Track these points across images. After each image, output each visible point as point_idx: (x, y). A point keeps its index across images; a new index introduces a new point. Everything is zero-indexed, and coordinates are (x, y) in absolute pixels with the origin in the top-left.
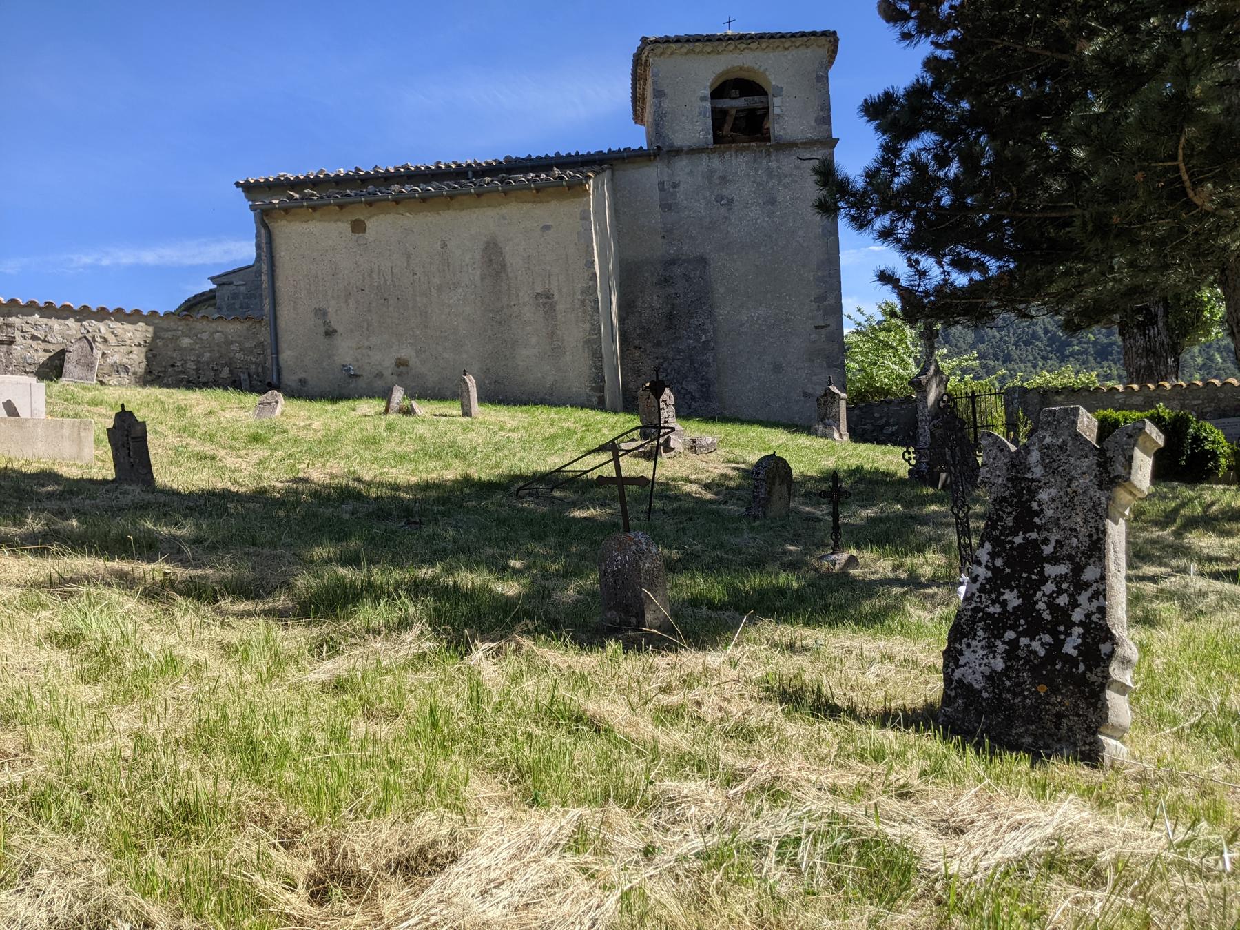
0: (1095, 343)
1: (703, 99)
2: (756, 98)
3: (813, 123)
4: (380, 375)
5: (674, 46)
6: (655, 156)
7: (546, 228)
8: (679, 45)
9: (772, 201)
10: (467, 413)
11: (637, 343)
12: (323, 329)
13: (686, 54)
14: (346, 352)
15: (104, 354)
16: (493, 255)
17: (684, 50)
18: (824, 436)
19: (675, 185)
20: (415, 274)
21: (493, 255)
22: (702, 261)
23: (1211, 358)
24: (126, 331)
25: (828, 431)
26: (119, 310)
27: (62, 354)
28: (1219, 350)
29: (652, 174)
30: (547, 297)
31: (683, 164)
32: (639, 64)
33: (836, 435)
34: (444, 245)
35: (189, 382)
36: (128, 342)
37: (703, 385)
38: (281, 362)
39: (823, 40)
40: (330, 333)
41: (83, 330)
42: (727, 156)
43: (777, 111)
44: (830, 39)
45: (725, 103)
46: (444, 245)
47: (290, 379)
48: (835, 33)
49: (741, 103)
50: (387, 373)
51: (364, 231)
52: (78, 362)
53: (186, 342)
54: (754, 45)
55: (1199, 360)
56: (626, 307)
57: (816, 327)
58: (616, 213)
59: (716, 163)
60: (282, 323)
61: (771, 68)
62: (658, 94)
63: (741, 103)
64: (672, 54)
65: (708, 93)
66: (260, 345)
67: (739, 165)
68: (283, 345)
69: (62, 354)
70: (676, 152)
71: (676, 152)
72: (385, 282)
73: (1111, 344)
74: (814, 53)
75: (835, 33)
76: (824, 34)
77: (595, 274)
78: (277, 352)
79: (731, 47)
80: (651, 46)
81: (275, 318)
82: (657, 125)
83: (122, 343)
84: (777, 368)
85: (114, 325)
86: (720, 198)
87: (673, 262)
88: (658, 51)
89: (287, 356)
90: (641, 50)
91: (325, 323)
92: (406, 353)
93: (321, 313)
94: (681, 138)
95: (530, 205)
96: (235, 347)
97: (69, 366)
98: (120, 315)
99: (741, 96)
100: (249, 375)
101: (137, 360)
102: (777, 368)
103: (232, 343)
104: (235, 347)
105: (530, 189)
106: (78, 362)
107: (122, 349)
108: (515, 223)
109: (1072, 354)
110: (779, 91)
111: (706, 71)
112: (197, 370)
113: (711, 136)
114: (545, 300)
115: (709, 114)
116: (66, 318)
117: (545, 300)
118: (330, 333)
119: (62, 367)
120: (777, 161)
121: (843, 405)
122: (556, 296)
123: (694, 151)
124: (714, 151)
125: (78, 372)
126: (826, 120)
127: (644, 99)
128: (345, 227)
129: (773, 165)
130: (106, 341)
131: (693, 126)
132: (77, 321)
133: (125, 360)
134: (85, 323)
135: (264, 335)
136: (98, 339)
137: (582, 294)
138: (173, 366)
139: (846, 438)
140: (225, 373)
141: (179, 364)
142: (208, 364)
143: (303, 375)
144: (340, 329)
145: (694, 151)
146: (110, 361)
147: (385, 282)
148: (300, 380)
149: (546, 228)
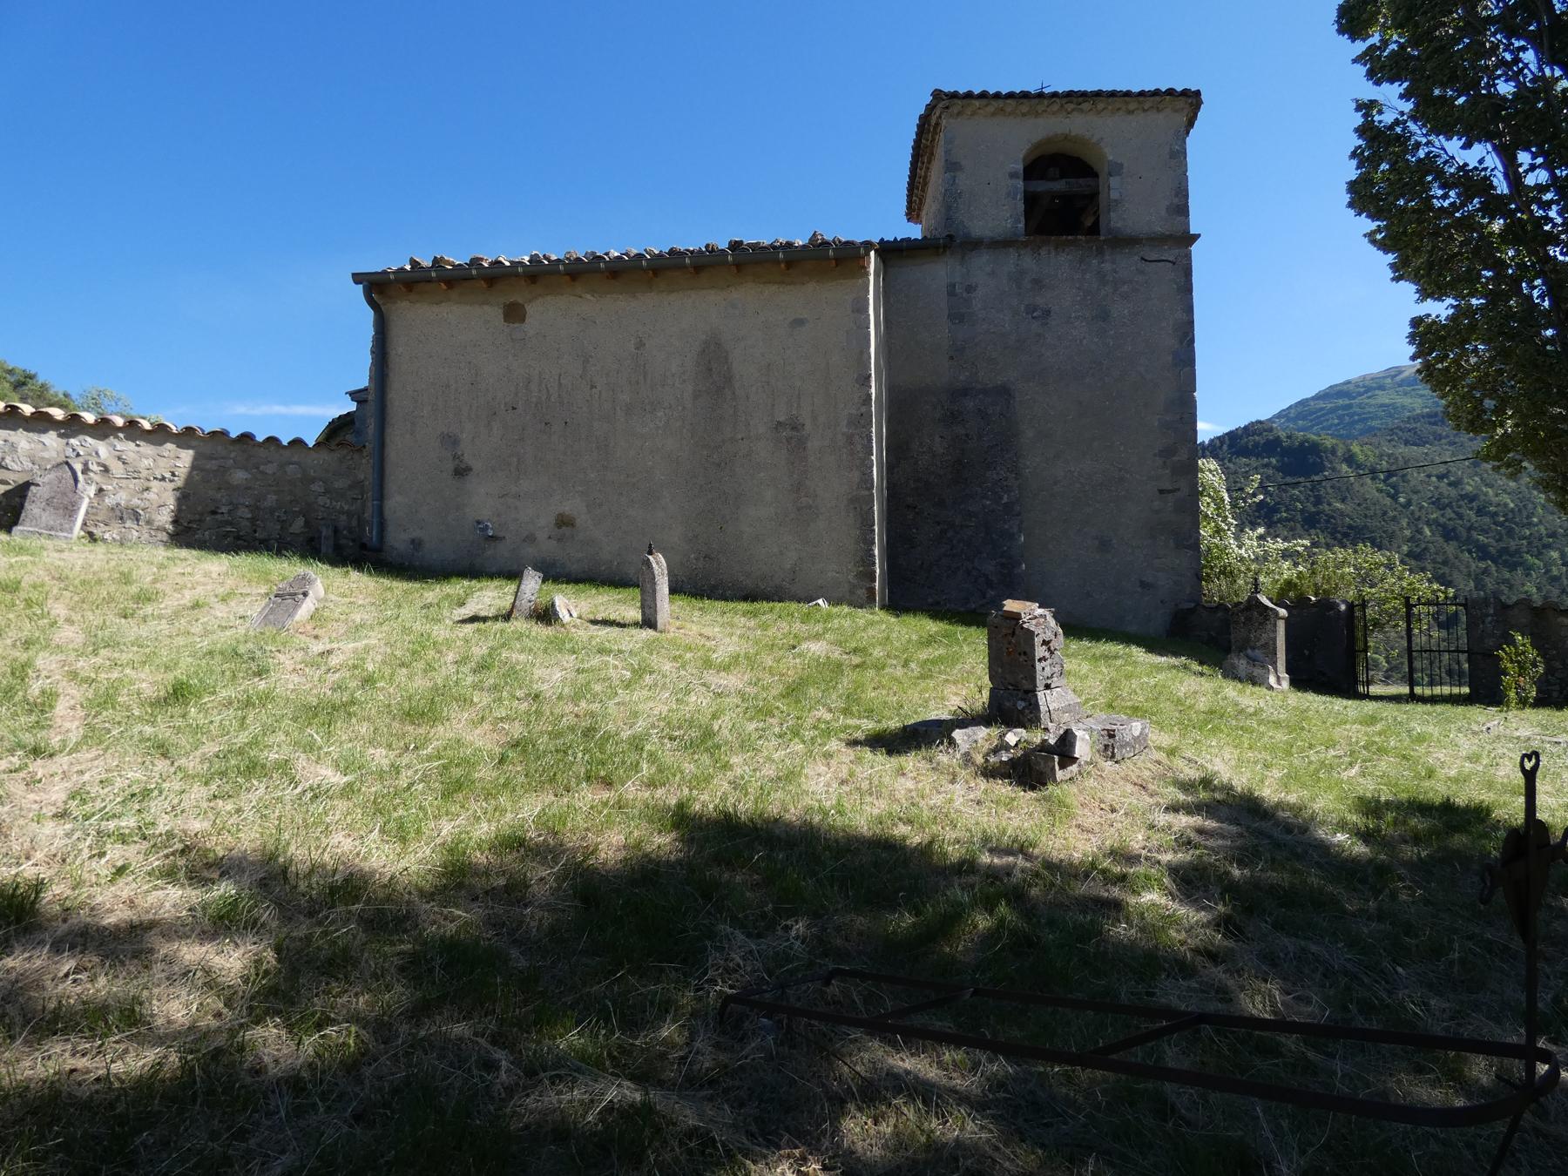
0: (1302, 511)
1: (1013, 175)
2: (1081, 181)
3: (1163, 213)
4: (531, 539)
5: (977, 103)
6: (945, 247)
7: (799, 322)
8: (984, 102)
9: (1104, 316)
10: (649, 622)
11: (910, 500)
12: (450, 466)
13: (993, 114)
14: (483, 501)
15: (101, 490)
16: (714, 367)
17: (991, 109)
18: (1254, 681)
19: (970, 289)
20: (593, 387)
21: (714, 367)
22: (1004, 392)
23: (1420, 531)
24: (142, 456)
25: (1257, 672)
26: (189, 431)
27: (22, 490)
28: (1428, 524)
29: (939, 273)
30: (794, 428)
31: (981, 263)
32: (927, 128)
33: (1272, 680)
34: (640, 345)
35: (238, 538)
36: (144, 473)
37: (1002, 565)
38: (387, 513)
39: (1181, 103)
40: (461, 472)
41: (69, 452)
42: (1043, 252)
43: (1114, 195)
44: (1192, 100)
45: (1041, 186)
46: (640, 345)
47: (398, 539)
48: (1198, 93)
49: (1059, 186)
50: (541, 536)
51: (522, 319)
52: (49, 502)
53: (239, 476)
54: (1086, 106)
55: (1407, 533)
56: (897, 451)
57: (1161, 492)
58: (886, 327)
59: (1028, 261)
60: (392, 454)
61: (1108, 138)
62: (952, 167)
63: (1059, 186)
64: (974, 114)
65: (1020, 167)
66: (358, 485)
67: (1060, 266)
68: (391, 486)
69: (22, 490)
70: (973, 245)
71: (973, 245)
72: (548, 398)
73: (1318, 513)
74: (1166, 120)
75: (1198, 93)
76: (1185, 93)
77: (870, 396)
78: (381, 496)
79: (1055, 107)
80: (946, 103)
81: (382, 445)
82: (949, 208)
83: (134, 474)
84: (1104, 545)
85: (127, 447)
86: (1031, 309)
87: (966, 392)
88: (955, 110)
89: (395, 503)
90: (930, 108)
91: (455, 457)
92: (572, 506)
93: (450, 441)
94: (980, 227)
95: (774, 288)
96: (317, 487)
97: (33, 509)
98: (160, 434)
99: (1062, 177)
100: (336, 531)
101: (163, 504)
102: (1104, 545)
103: (313, 480)
104: (317, 487)
105: (778, 262)
106: (49, 502)
107: (132, 484)
108: (749, 316)
109: (1280, 521)
110: (1116, 169)
111: (1018, 140)
112: (253, 520)
113: (1021, 225)
114: (791, 434)
115: (1020, 196)
116: (45, 431)
117: (791, 434)
118: (461, 472)
119: (22, 506)
120: (1113, 262)
121: (1281, 626)
122: (808, 427)
123: (1001, 244)
124: (1025, 245)
125: (47, 517)
126: (1182, 210)
127: (925, 184)
128: (494, 313)
129: (1107, 266)
130: (106, 470)
131: (997, 208)
132: (60, 436)
133: (135, 501)
134: (73, 441)
135: (365, 470)
136: (94, 467)
137: (849, 424)
138: (214, 513)
139: (1285, 684)
140: (298, 525)
141: (224, 509)
142: (272, 511)
143: (417, 534)
144: (477, 465)
145: (1001, 244)
146: (109, 501)
147: (548, 398)
148: (413, 541)
149: (799, 322)
